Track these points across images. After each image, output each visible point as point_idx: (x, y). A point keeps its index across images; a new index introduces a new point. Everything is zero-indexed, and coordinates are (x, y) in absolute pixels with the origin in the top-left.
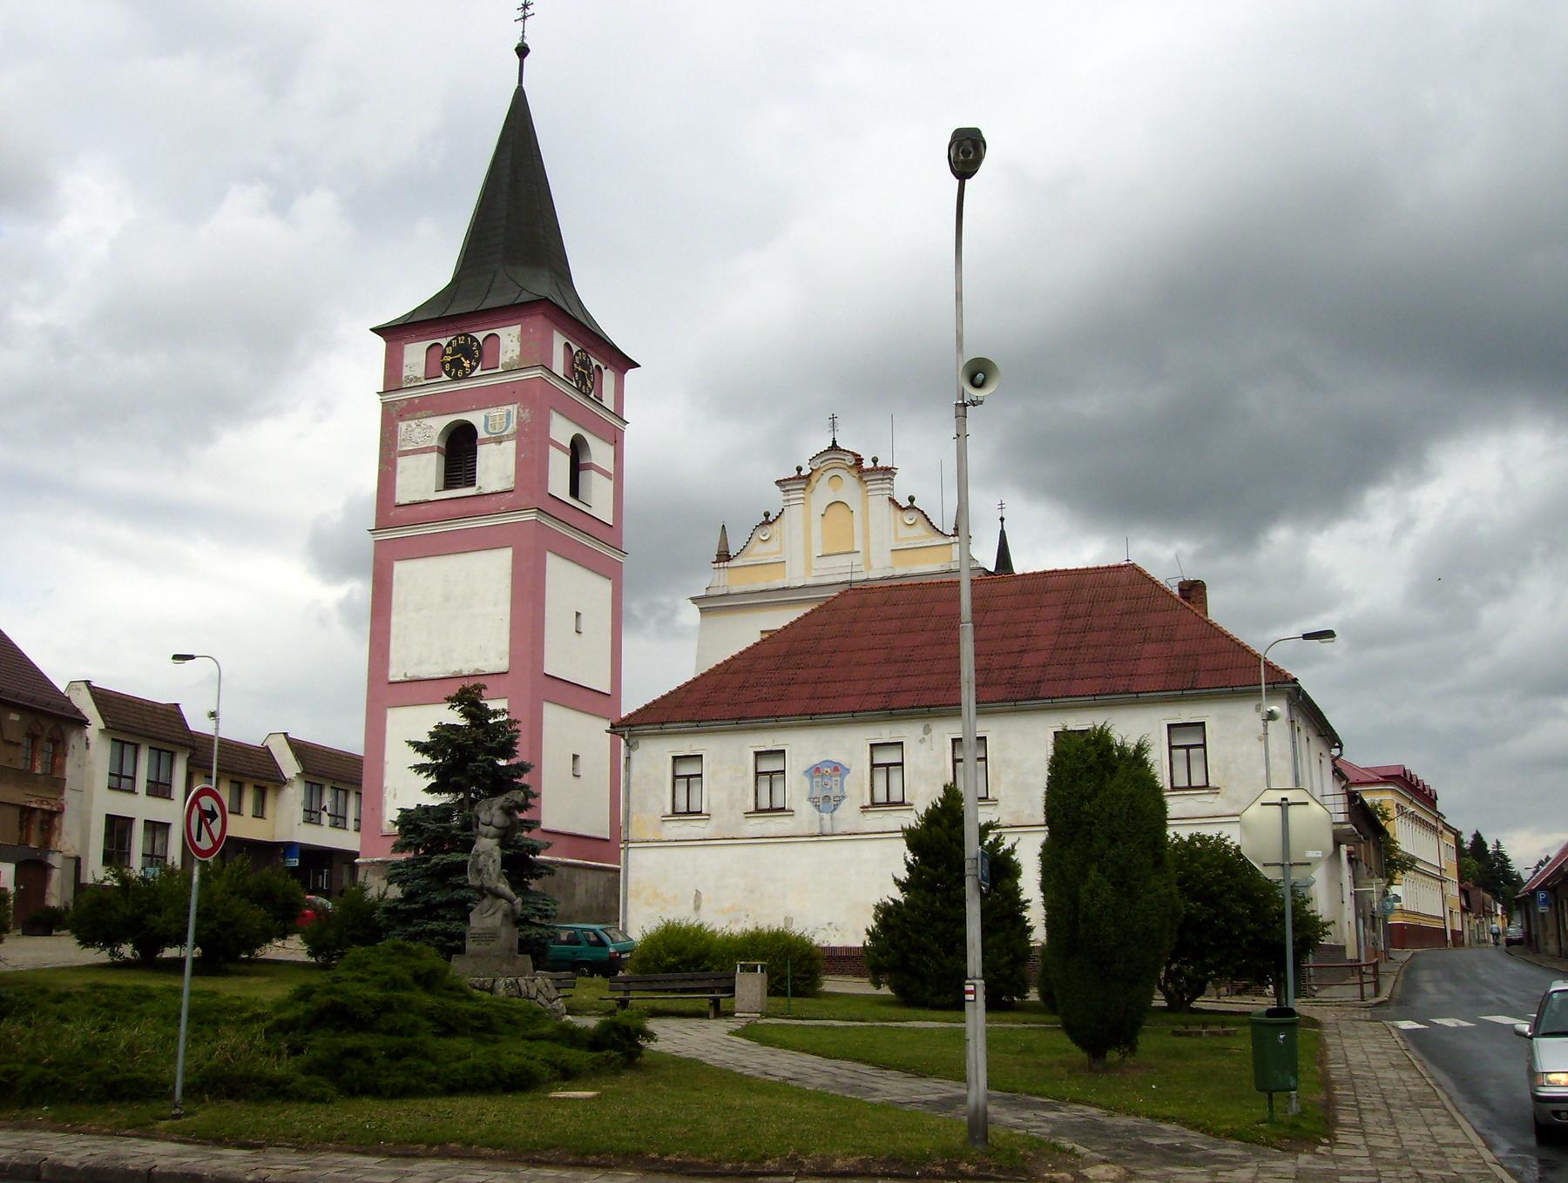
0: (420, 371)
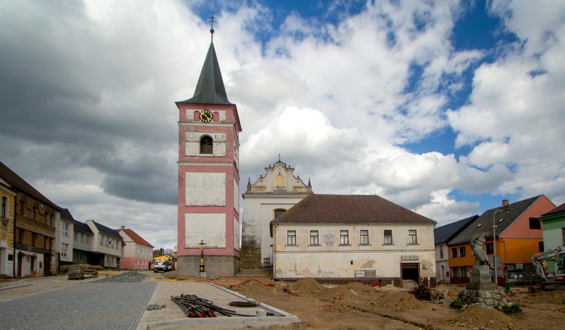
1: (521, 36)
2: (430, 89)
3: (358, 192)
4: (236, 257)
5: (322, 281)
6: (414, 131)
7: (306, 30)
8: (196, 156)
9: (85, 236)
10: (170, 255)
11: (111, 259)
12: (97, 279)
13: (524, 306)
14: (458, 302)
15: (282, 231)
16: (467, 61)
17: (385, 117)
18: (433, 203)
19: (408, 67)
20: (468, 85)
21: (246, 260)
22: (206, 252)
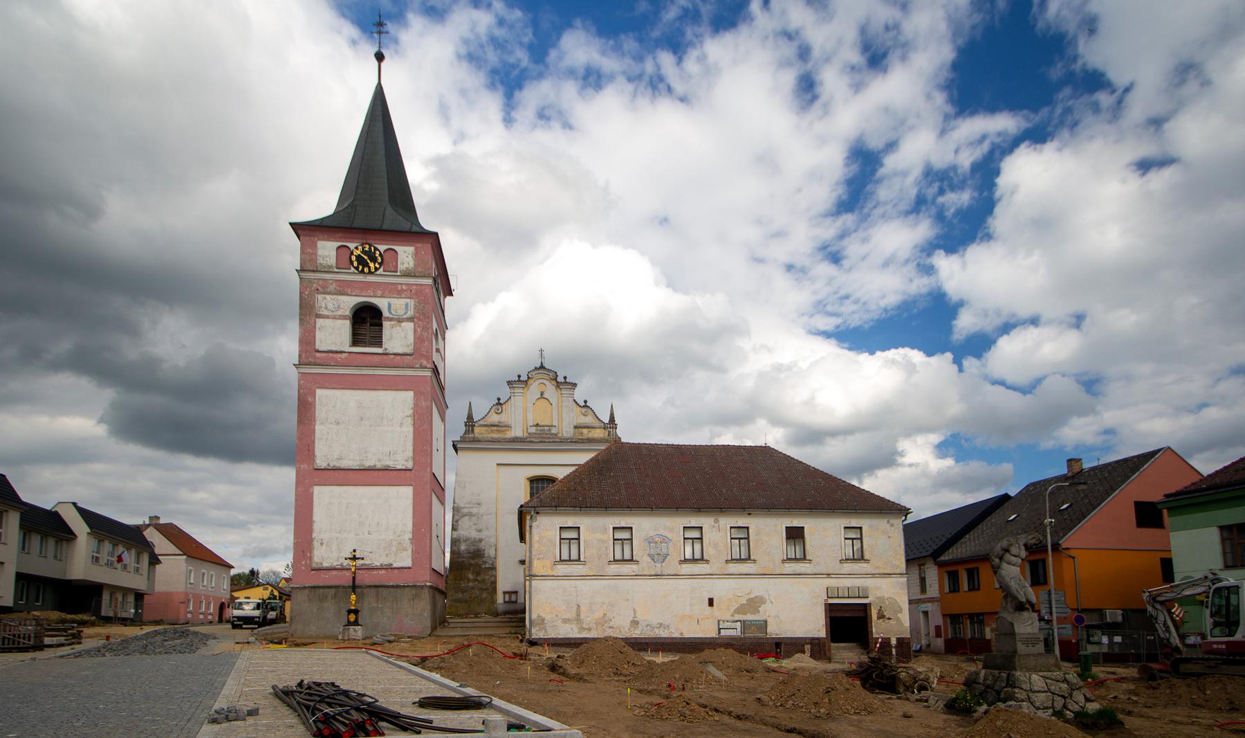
0: (332, 261)
1: (1118, 77)
2: (895, 205)
3: (727, 438)
4: (435, 589)
5: (641, 645)
6: (856, 302)
7: (609, 64)
8: (341, 352)
9: (51, 542)
10: (275, 586)
11: (119, 597)
12: (78, 648)
13: (1129, 713)
14: (965, 698)
15: (547, 527)
16: (983, 138)
17: (790, 268)
18: (901, 465)
19: (845, 155)
20: (986, 193)
21: (460, 595)
22: (364, 578)
